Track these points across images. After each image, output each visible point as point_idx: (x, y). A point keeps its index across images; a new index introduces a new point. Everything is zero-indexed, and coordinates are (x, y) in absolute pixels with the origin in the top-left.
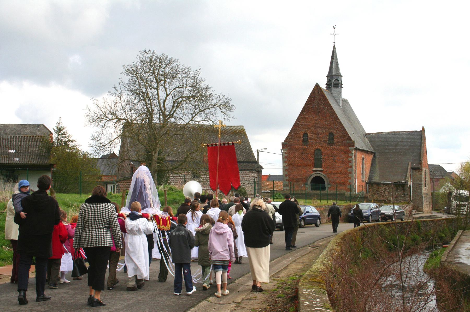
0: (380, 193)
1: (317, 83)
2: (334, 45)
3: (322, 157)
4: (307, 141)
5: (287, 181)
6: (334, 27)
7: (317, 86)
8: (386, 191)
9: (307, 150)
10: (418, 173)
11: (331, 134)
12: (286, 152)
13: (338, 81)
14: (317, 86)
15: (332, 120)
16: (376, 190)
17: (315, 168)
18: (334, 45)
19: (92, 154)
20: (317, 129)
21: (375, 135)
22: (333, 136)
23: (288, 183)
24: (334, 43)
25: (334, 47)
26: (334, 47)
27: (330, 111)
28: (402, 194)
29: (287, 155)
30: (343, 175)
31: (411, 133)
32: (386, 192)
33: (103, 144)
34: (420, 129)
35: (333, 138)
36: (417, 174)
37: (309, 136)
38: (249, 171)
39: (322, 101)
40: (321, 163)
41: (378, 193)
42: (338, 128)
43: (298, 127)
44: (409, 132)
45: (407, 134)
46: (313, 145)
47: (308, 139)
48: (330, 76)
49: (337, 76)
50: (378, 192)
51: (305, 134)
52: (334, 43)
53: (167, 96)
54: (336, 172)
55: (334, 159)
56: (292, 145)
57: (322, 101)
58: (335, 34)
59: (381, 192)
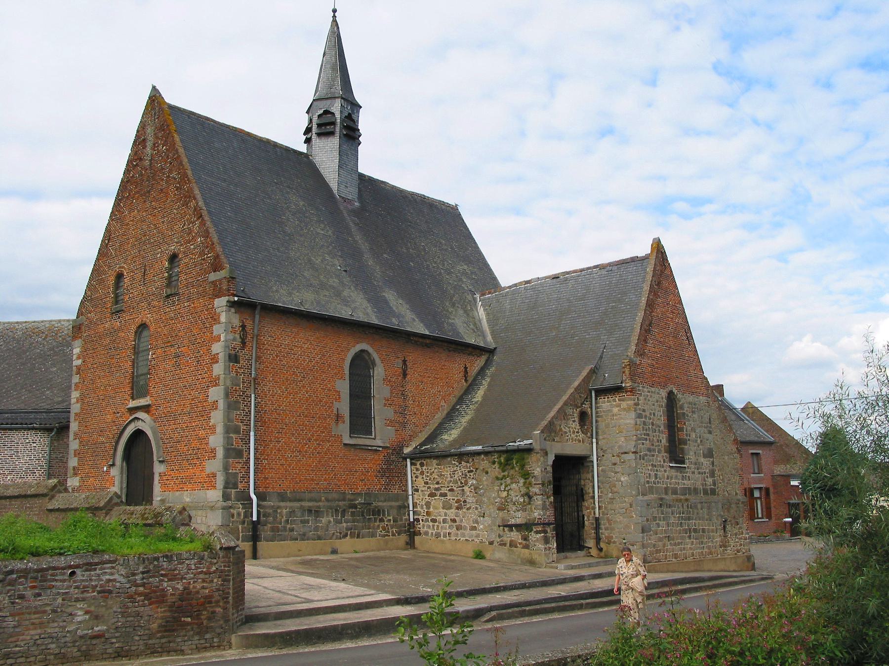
0: (449, 493)
2: (334, 16)
10: (619, 406)
11: (173, 258)
13: (333, 114)
16: (438, 483)
17: (133, 399)
21: (508, 292)
24: (334, 11)
31: (615, 268)
32: (466, 488)
34: (643, 249)
36: (615, 410)
38: (17, 429)
44: (610, 264)
45: (604, 272)
49: (329, 102)
50: (443, 490)
51: (119, 277)
52: (334, 11)
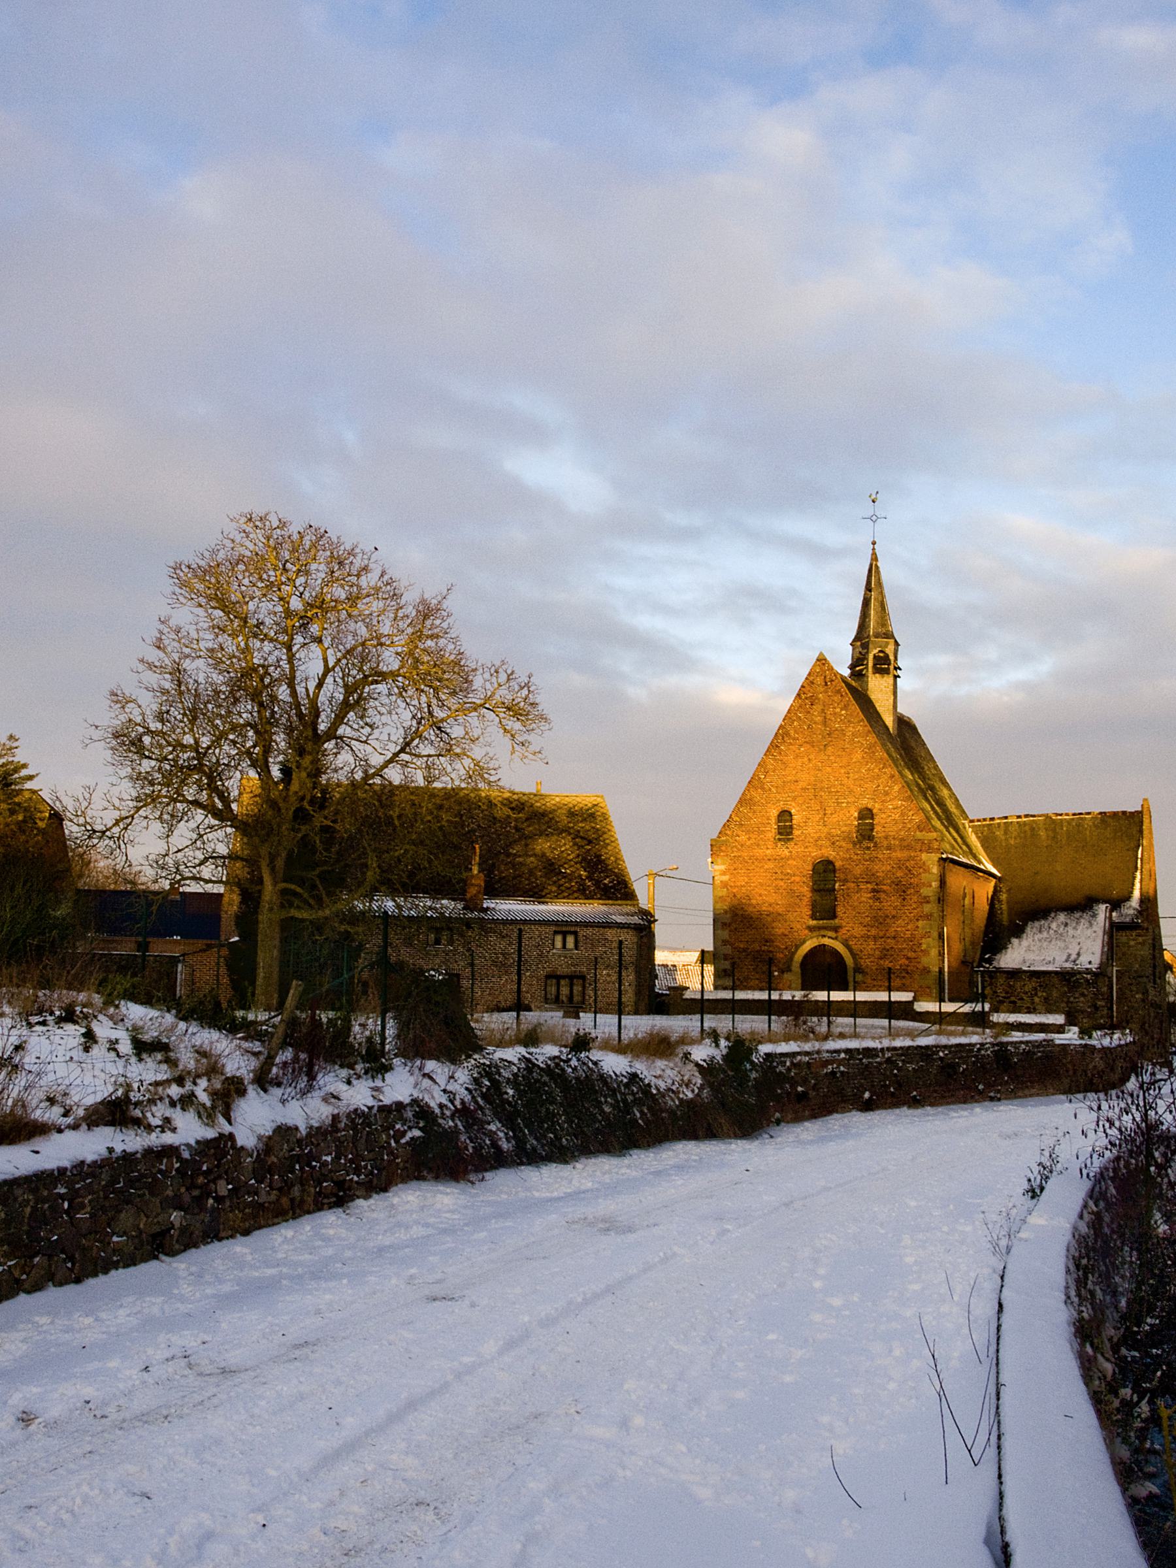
1: (821, 654)
2: (874, 549)
3: (837, 885)
4: (791, 833)
5: (725, 959)
6: (873, 497)
7: (822, 660)
8: (1036, 994)
9: (790, 862)
12: (723, 867)
14: (822, 660)
15: (869, 769)
18: (874, 549)
19: (335, 681)
20: (821, 796)
22: (872, 818)
23: (730, 952)
24: (874, 543)
25: (874, 558)
26: (874, 558)
27: (860, 739)
28: (1089, 1007)
29: (726, 878)
30: (905, 941)
32: (1036, 999)
33: (98, 827)
35: (872, 824)
36: (1132, 943)
37: (796, 819)
39: (838, 710)
40: (835, 905)
41: (1011, 1002)
42: (887, 793)
43: (763, 789)
46: (807, 847)
47: (791, 827)
48: (861, 639)
50: (1013, 999)
51: (785, 815)
52: (874, 543)
53: (327, 670)
54: (881, 934)
55: (874, 891)
56: (742, 846)
57: (838, 710)
58: (874, 519)
59: (1022, 999)
